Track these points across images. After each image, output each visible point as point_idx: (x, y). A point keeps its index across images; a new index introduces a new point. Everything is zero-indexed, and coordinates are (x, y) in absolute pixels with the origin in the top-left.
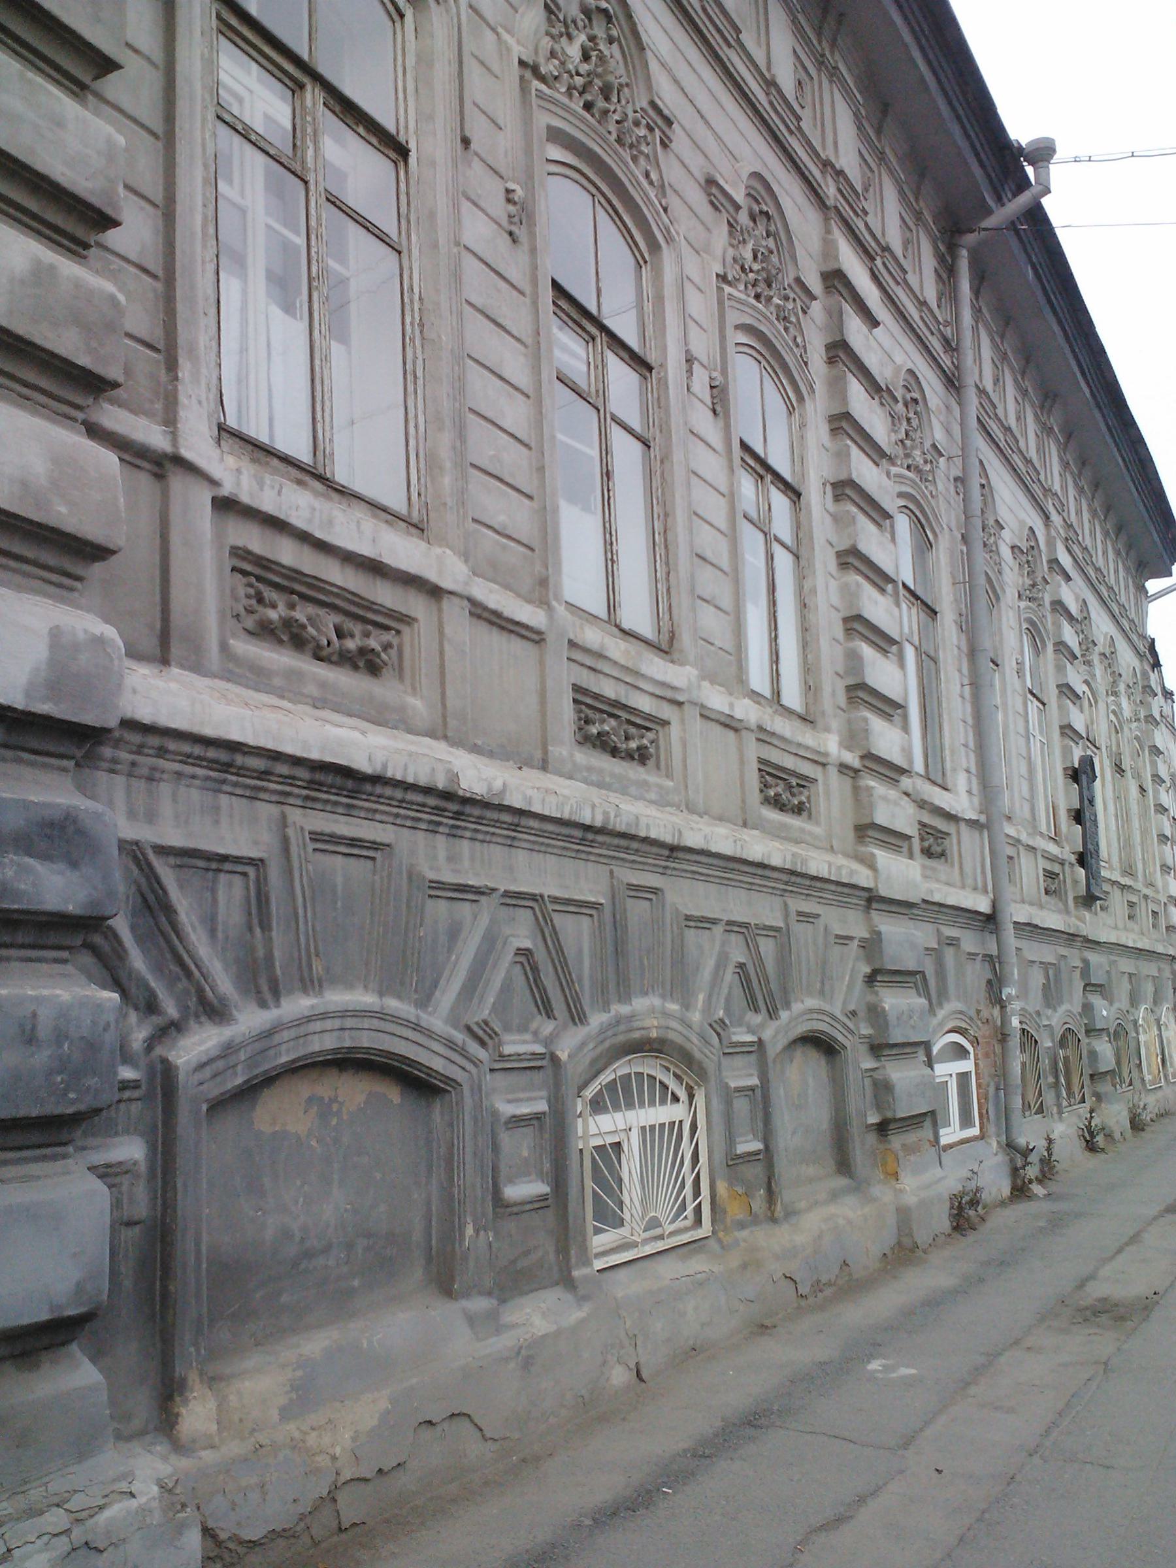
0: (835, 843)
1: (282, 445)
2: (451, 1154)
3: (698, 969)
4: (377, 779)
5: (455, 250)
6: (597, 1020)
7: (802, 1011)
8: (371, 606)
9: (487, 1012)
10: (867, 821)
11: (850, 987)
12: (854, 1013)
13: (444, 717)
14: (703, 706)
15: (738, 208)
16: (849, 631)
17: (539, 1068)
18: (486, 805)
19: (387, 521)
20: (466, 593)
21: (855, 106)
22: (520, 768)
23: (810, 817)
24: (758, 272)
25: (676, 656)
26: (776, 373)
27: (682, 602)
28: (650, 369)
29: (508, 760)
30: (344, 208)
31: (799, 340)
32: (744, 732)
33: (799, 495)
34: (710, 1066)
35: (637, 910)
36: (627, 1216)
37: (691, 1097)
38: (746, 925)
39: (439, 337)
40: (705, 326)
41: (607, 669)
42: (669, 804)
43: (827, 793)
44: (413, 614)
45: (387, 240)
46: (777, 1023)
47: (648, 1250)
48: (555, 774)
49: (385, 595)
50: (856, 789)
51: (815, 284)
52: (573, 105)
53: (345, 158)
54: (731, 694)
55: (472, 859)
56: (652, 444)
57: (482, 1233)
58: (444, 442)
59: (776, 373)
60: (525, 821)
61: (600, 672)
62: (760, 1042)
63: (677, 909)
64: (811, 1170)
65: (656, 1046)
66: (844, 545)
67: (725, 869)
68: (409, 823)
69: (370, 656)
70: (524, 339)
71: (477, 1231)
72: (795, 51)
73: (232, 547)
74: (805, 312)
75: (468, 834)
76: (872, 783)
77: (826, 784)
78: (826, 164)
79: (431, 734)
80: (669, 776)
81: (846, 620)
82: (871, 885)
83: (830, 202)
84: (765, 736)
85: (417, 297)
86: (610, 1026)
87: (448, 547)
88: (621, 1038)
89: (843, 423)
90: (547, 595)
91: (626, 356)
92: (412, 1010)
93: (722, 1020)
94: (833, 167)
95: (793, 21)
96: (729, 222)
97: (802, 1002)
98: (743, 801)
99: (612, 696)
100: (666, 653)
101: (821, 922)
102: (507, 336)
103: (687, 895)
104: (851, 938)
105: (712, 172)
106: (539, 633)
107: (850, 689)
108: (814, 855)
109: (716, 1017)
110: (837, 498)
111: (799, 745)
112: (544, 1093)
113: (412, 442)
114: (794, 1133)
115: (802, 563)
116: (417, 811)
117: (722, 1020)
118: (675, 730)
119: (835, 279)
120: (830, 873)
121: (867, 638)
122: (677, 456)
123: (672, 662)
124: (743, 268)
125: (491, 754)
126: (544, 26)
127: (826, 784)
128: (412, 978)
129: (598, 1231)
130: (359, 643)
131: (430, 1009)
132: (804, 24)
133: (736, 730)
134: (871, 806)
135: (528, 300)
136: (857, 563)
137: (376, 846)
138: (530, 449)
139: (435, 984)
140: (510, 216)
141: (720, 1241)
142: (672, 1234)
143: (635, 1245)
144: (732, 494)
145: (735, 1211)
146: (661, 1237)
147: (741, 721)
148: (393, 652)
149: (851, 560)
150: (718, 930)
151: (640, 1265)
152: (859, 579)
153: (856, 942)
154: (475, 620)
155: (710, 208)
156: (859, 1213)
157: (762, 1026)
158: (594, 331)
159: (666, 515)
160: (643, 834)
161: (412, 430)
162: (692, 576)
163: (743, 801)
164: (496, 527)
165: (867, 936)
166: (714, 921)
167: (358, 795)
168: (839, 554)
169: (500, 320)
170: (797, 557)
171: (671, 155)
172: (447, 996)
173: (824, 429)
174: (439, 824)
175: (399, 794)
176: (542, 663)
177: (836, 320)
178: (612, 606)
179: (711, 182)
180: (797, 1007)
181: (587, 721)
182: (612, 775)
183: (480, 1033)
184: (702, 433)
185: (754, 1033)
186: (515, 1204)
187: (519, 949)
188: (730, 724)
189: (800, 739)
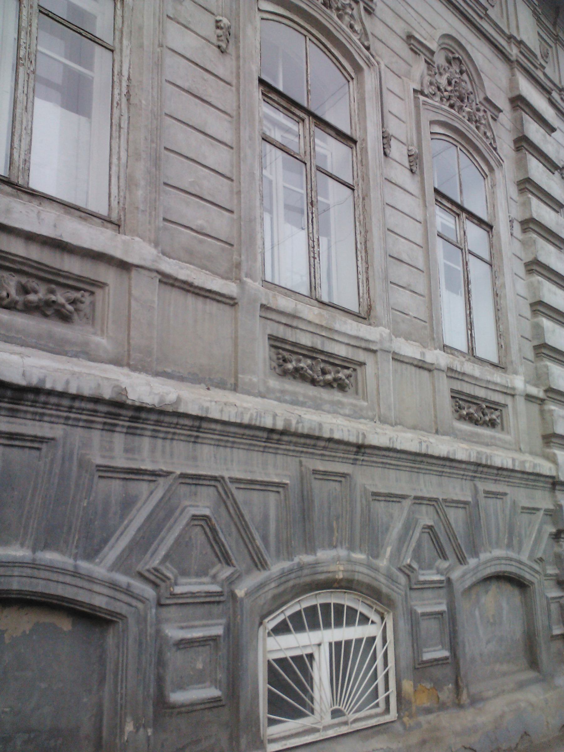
0: (522, 447)
1: (92, 207)
2: (117, 668)
3: (387, 529)
4: (37, 390)
5: (159, 50)
6: (277, 567)
7: (493, 556)
8: (58, 273)
9: (157, 562)
10: (549, 432)
11: (537, 541)
12: (541, 559)
13: (129, 351)
14: (394, 353)
15: (432, 53)
16: (535, 312)
17: (219, 603)
18: (162, 412)
19: (80, 217)
20: (153, 267)
21: (533, 6)
22: (208, 389)
23: (503, 429)
24: (451, 91)
25: (372, 321)
26: (471, 153)
27: (377, 287)
28: (355, 142)
29: (200, 383)
30: (58, 19)
31: (489, 134)
32: (435, 372)
33: (491, 227)
34: (398, 598)
35: (322, 490)
36: (316, 707)
37: (383, 618)
38: (436, 500)
39: (140, 101)
40: (404, 119)
41: (302, 325)
42: (362, 417)
43: (516, 413)
44: (102, 280)
45: (100, 42)
46: (464, 567)
47: (331, 733)
48: (243, 393)
49: (73, 265)
50: (542, 412)
51: (502, 102)
52: (443, 106)
53: (330, 151)
54: (424, 347)
55: (163, 452)
56: (356, 188)
57: (142, 730)
58: (140, 169)
59: (471, 153)
60: (205, 425)
61: (296, 328)
62: (449, 580)
63: (365, 488)
64: (505, 667)
65: (343, 584)
66: (530, 258)
67: (414, 461)
68: (416, 470)
69: (470, 416)
70: (229, 111)
71: (137, 728)
72: (539, 34)
73: (269, 335)
74: (495, 120)
75: (162, 435)
76: (553, 407)
77: (514, 408)
78: (510, 38)
79: (117, 362)
80: (365, 398)
81: (532, 305)
82: (554, 473)
83: (513, 58)
84: (452, 373)
85: (125, 78)
86: (291, 571)
87: (138, 236)
88: (308, 579)
89: (527, 185)
90: (240, 273)
91: (333, 133)
92: (71, 561)
93: (410, 566)
94: (515, 38)
95: (537, 20)
96: (426, 61)
97: (491, 552)
98: (436, 417)
99: (309, 344)
100: (365, 319)
101: (508, 499)
102: (213, 109)
103: (371, 478)
104: (538, 509)
105: (410, 30)
106: (232, 298)
107: (536, 348)
108: (496, 452)
109: (404, 563)
110: (524, 231)
111: (489, 382)
112: (223, 621)
113: (114, 168)
114: (488, 642)
115: (494, 269)
116: (250, 440)
117: (410, 566)
118: (370, 369)
119: (519, 102)
120: (514, 465)
121: (546, 314)
122: (374, 195)
123: (370, 325)
124: (439, 89)
125: (181, 379)
126: (426, 71)
127: (514, 408)
128: (74, 537)
129: (271, 722)
130: (334, 376)
131: (97, 560)
132: (548, 26)
133: (430, 371)
134: (553, 423)
135: (234, 89)
136: (539, 269)
137: (42, 440)
138: (232, 180)
139: (105, 541)
140: (218, 36)
141: (403, 724)
142: (355, 721)
143: (317, 730)
144: (426, 221)
145: (424, 701)
146: (346, 723)
147: (432, 364)
148: (352, 379)
149: (535, 267)
150: (407, 503)
151: (320, 745)
152: (540, 278)
153: (542, 512)
154: (163, 286)
155: (411, 53)
156: (542, 697)
157: (449, 569)
158: (302, 115)
159: (366, 232)
160: (327, 435)
161: (115, 161)
162: (386, 270)
163: (436, 417)
164: (194, 227)
165: (552, 507)
166: (404, 497)
167: (22, 402)
168: (527, 265)
169: (205, 98)
170: (491, 265)
171: (499, 124)
172: (113, 552)
173: (513, 191)
174: (116, 425)
175: (175, 420)
176: (236, 318)
177: (519, 124)
178: (313, 287)
179: (410, 37)
180: (484, 556)
181: (285, 360)
182: (305, 396)
183: (152, 577)
184: (399, 181)
185: (442, 574)
186: (182, 706)
187: (194, 516)
188: (422, 366)
189: (489, 378)
